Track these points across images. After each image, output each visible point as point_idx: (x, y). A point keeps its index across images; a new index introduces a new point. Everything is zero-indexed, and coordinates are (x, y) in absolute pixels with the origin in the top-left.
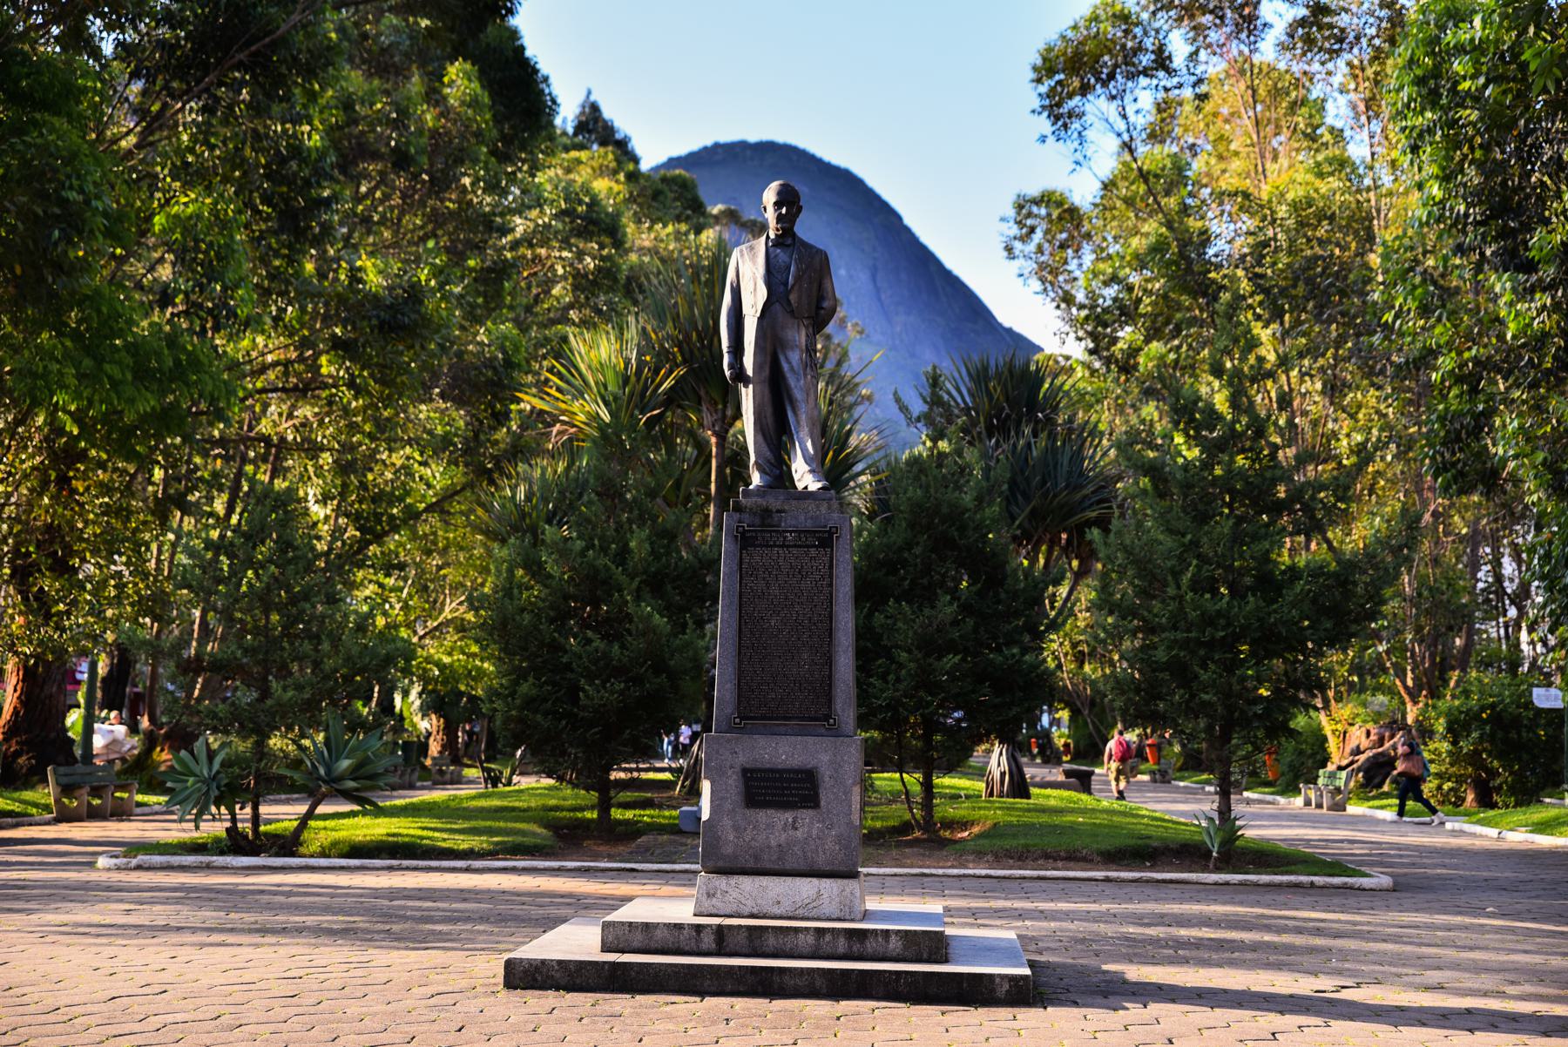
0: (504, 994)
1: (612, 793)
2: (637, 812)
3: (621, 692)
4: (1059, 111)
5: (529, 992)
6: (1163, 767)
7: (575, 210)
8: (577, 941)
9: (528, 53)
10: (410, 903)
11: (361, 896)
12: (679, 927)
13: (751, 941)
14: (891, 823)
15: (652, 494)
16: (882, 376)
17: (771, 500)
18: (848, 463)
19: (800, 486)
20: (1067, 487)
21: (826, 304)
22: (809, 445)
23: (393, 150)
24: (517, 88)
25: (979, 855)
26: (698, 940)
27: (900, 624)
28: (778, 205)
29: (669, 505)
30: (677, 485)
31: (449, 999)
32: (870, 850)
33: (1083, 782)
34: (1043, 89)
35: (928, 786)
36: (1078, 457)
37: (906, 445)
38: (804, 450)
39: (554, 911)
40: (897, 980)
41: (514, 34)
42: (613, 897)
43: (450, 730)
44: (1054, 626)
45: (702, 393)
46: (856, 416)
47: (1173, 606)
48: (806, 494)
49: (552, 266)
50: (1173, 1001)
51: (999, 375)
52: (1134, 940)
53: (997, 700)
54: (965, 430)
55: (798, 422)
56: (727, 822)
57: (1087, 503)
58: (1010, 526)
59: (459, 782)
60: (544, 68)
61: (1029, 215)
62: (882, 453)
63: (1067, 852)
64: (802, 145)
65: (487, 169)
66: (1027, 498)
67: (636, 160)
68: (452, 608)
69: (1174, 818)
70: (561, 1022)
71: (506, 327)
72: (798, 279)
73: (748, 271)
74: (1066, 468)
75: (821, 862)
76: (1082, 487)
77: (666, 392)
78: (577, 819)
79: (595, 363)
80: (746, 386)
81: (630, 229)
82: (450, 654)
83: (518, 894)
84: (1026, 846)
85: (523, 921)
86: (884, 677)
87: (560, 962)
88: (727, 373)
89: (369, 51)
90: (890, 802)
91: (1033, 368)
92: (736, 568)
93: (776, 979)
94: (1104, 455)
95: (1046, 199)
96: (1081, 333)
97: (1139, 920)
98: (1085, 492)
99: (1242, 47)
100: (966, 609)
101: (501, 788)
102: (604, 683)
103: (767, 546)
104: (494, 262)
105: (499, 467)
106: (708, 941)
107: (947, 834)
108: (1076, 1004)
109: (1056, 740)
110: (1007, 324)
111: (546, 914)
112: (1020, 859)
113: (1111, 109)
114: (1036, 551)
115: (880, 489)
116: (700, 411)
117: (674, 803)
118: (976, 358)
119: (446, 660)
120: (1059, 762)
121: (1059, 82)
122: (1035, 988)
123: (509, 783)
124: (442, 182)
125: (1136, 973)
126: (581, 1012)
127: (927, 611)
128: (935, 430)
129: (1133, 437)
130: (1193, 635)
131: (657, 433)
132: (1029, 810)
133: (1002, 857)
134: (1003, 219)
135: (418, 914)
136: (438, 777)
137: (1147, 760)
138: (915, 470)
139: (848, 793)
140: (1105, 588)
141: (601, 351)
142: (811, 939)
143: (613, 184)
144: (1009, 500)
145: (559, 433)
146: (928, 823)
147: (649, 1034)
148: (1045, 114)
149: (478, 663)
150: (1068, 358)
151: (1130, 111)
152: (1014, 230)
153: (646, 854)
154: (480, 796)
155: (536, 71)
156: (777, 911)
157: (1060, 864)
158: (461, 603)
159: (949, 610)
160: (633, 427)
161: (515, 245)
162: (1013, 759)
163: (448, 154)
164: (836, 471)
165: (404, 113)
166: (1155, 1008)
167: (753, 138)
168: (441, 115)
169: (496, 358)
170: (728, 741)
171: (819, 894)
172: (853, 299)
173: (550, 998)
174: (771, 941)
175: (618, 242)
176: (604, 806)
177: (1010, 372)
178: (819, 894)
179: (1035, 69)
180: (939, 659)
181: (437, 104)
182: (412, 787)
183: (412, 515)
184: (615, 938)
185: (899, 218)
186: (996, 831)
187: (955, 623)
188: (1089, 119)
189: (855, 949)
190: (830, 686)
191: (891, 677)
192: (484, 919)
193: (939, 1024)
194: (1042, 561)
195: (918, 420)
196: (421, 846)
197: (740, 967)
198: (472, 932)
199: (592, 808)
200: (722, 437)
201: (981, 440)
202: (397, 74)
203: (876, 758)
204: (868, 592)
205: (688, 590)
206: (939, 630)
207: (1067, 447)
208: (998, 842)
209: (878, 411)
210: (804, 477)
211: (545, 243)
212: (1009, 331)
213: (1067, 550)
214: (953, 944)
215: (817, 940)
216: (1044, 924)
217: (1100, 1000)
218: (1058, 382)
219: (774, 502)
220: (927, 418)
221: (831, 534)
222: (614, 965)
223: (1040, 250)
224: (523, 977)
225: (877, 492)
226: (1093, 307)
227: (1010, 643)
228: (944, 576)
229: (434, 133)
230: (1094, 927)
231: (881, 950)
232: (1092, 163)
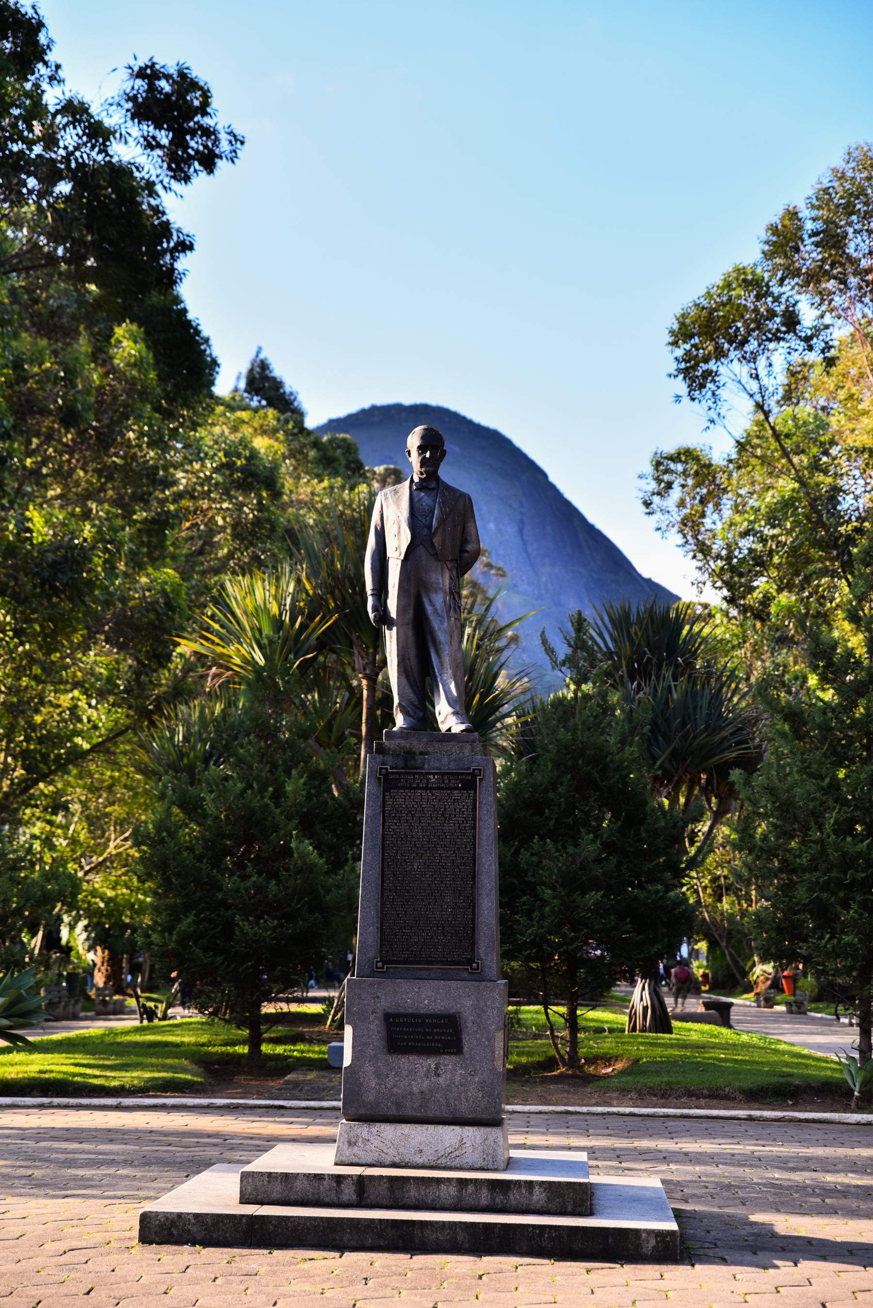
0: (139, 1250)
1: (263, 1027)
2: (288, 1047)
3: (274, 929)
4: (696, 376)
5: (165, 1248)
6: (799, 998)
7: (234, 463)
8: (214, 1192)
9: (190, 316)
10: (57, 1145)
11: (8, 1137)
12: (319, 1177)
13: (392, 1192)
14: (536, 1059)
15: (304, 734)
16: (523, 612)
17: (415, 743)
18: (495, 705)
19: (443, 728)
20: (706, 728)
21: (469, 547)
22: (453, 686)
23: (60, 408)
24: (182, 355)
25: (624, 1093)
26: (339, 1192)
27: (546, 862)
28: (422, 449)
29: (321, 745)
30: (329, 727)
31: (80, 1256)
32: (515, 1086)
33: (721, 1014)
34: (679, 352)
35: (572, 1021)
36: (717, 699)
37: (550, 688)
38: (448, 693)
39: (199, 1153)
40: (541, 1235)
41: (178, 300)
42: (260, 1137)
43: (113, 961)
44: (693, 863)
45: (354, 638)
46: (502, 660)
47: (815, 848)
48: (449, 736)
49: (213, 517)
50: (824, 1258)
51: (640, 621)
52: (780, 1187)
53: (639, 938)
54: (608, 674)
55: (442, 664)
56: (369, 1068)
57: (726, 744)
58: (650, 768)
59: (123, 1013)
60: (206, 330)
61: (667, 471)
62: (528, 696)
63: (710, 1089)
64: (453, 407)
65: (150, 426)
66: (668, 740)
67: (299, 414)
68: (116, 844)
69: (813, 1052)
70: (195, 1282)
71: (169, 573)
72: (441, 522)
73: (392, 515)
74: (705, 711)
75: (465, 1110)
76: (722, 729)
77: (318, 638)
78: (228, 1054)
79: (250, 608)
80: (390, 629)
81: (288, 483)
82: (114, 888)
83: (165, 1134)
84: (669, 1083)
85: (167, 1164)
86: (529, 915)
87: (197, 1216)
88: (371, 616)
89: (39, 314)
90: (536, 1037)
91: (672, 615)
92: (379, 810)
93: (417, 1232)
94: (739, 702)
95: (686, 455)
96: (719, 584)
97: (783, 1164)
98: (725, 733)
99: (866, 310)
100: (608, 846)
101: (156, 1022)
102: (259, 918)
103: (411, 788)
104: (158, 514)
105: (158, 709)
106: (349, 1192)
107: (592, 1069)
108: (724, 1261)
109: (695, 970)
110: (646, 575)
111: (190, 1157)
112: (663, 1096)
113: (743, 370)
114: (677, 789)
115: (526, 731)
116: (351, 654)
117: (325, 1038)
118: (617, 605)
119: (110, 893)
120: (698, 992)
121: (694, 346)
122: (682, 1243)
123: (165, 1017)
124: (106, 440)
125: (787, 1224)
126: (216, 1270)
127: (571, 849)
128: (578, 673)
129: (767, 683)
130: (834, 874)
131: (312, 676)
132: (672, 1046)
133: (645, 1095)
134: (640, 477)
135: (62, 1157)
136: (101, 1007)
137: (783, 991)
138: (560, 711)
139: (491, 1039)
140: (745, 829)
141: (259, 596)
142: (453, 1190)
143: (272, 442)
144: (650, 742)
145: (216, 676)
146: (573, 1060)
147: (285, 1296)
148: (681, 376)
149: (141, 897)
150: (706, 606)
151: (762, 372)
152: (653, 486)
153: (295, 1091)
154: (137, 1030)
155: (198, 332)
156: (419, 1160)
157: (703, 1102)
158: (126, 839)
159: (591, 848)
160: (286, 671)
161: (178, 497)
162: (656, 995)
163: (115, 410)
164: (480, 711)
165: (72, 373)
166: (808, 1267)
167: (407, 401)
168: (106, 374)
169: (157, 602)
170: (371, 985)
171: (462, 1143)
172: (502, 551)
173: (186, 1254)
174: (413, 1193)
175: (276, 494)
176: (255, 1041)
177: (651, 617)
178: (462, 1143)
179: (672, 332)
180: (584, 894)
181: (103, 364)
182: (75, 1017)
183: (77, 756)
184: (255, 1188)
185: (545, 476)
186: (635, 1067)
187: (599, 860)
188: (721, 379)
189: (498, 1200)
190: (473, 929)
191: (536, 914)
192: (128, 1163)
193: (584, 1285)
194: (682, 800)
195: (563, 664)
196: (73, 1083)
197: (381, 1221)
198: (114, 1176)
199: (243, 1043)
200: (372, 681)
201: (623, 684)
202: (66, 335)
203: (521, 990)
204: (513, 830)
205: (335, 827)
206: (582, 868)
207: (707, 691)
208: (642, 1080)
209: (525, 656)
210: (447, 719)
211: (206, 495)
212: (649, 581)
213: (706, 791)
214: (598, 1193)
215: (460, 1191)
216: (689, 1168)
217: (748, 1257)
218: (696, 629)
219: (417, 744)
220: (570, 661)
221: (474, 775)
222: (252, 1219)
223: (681, 504)
224: (160, 1231)
225: (523, 733)
226: (729, 558)
227: (653, 880)
228: (587, 814)
229: (100, 389)
230: (739, 1171)
231: (524, 1202)
232: (726, 421)
